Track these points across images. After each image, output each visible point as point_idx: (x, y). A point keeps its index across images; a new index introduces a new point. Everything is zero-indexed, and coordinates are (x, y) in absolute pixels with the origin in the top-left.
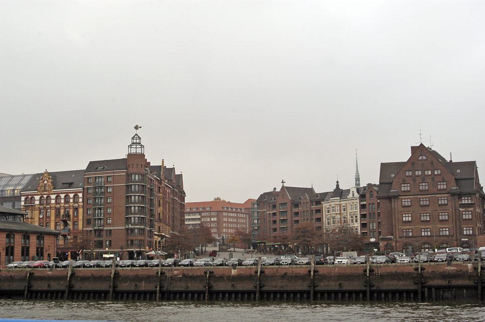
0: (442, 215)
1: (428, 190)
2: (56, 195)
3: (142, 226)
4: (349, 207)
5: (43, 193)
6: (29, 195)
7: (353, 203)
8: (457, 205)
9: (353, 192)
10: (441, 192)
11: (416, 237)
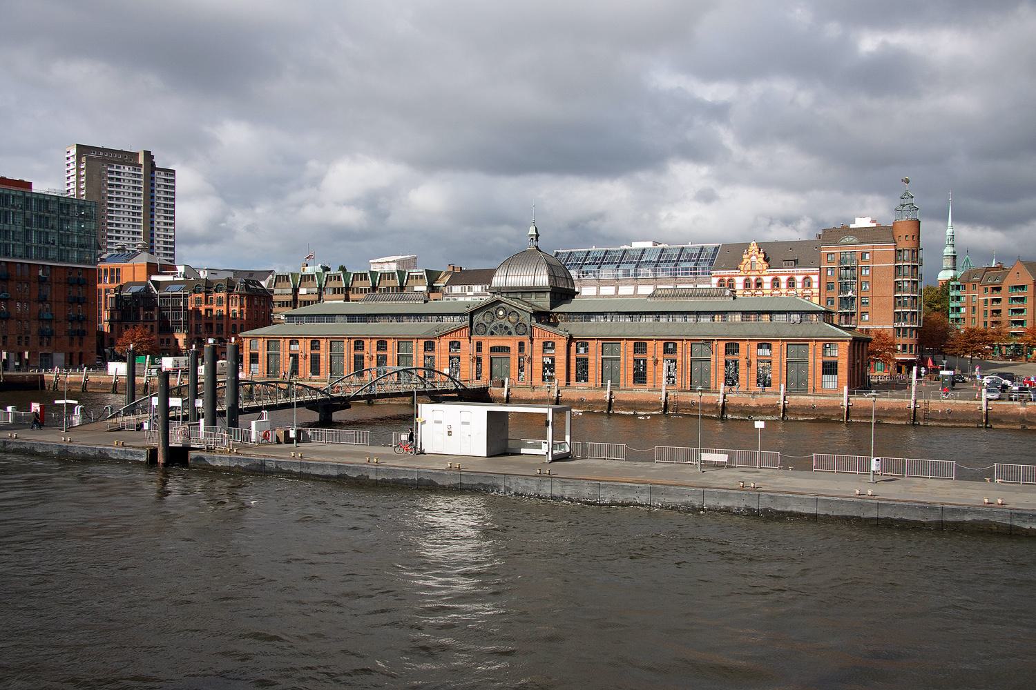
2: (719, 278)
5: (749, 273)
6: (725, 276)
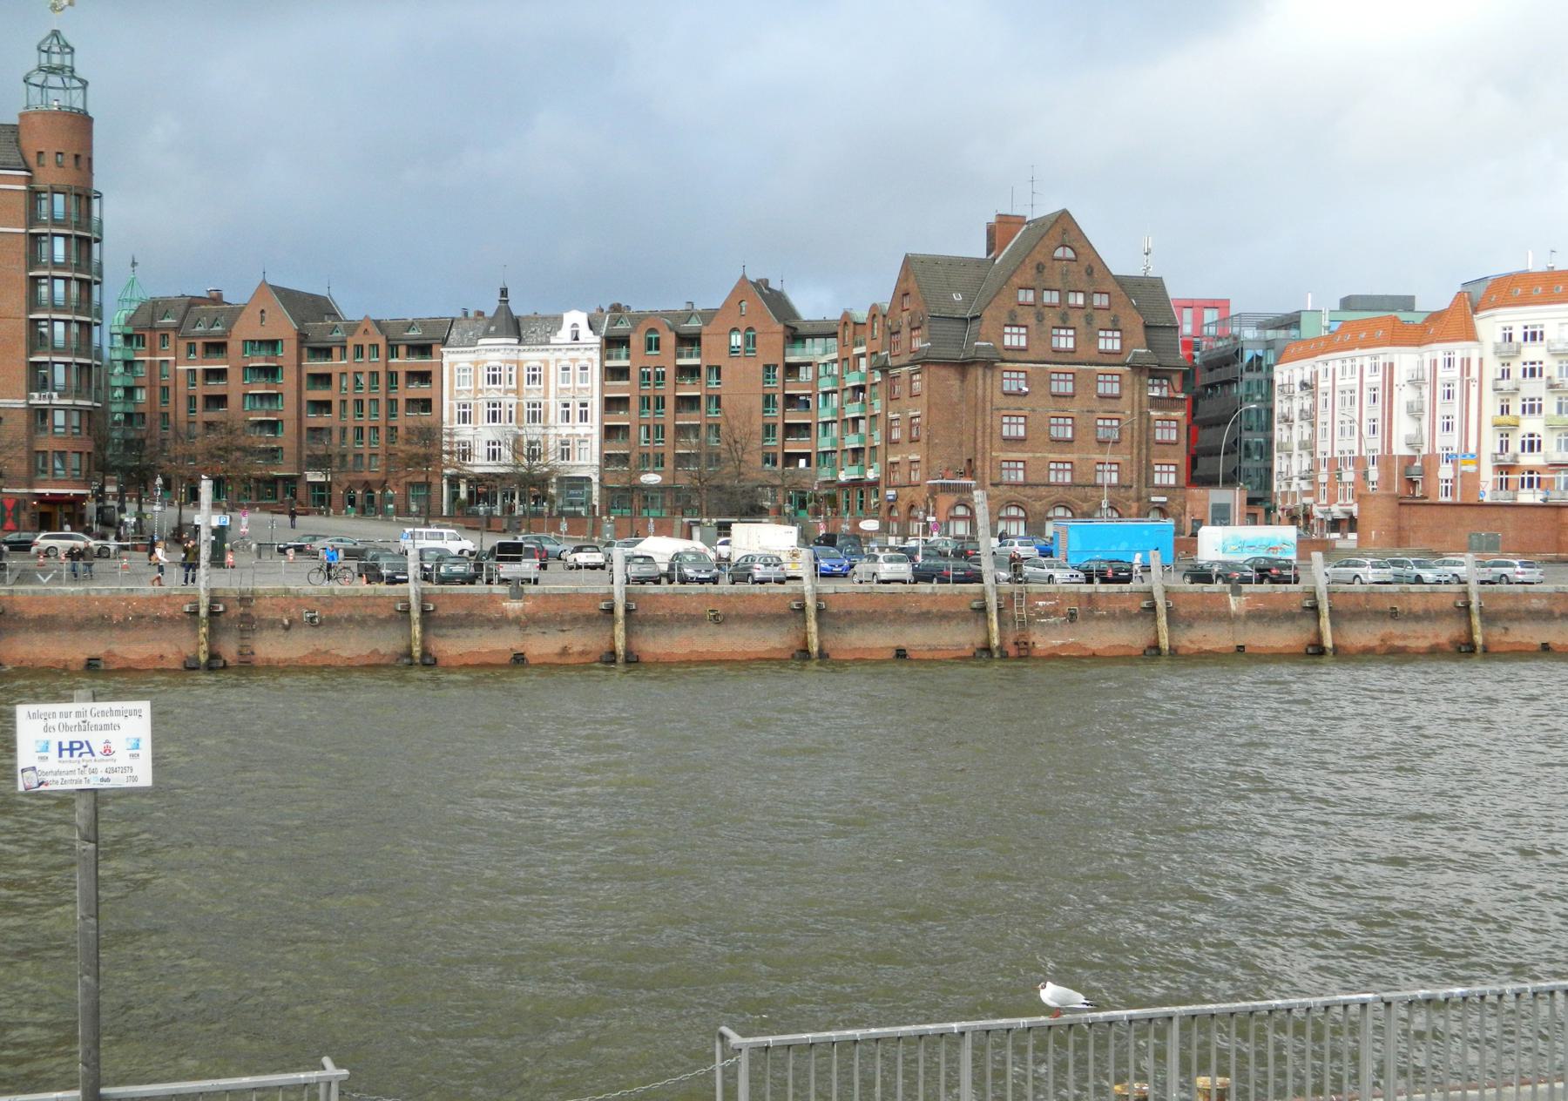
0: (1010, 424)
1: (1073, 352)
3: (82, 398)
4: (554, 375)
7: (574, 360)
8: (1145, 401)
9: (575, 325)
10: (1107, 359)
11: (1037, 485)
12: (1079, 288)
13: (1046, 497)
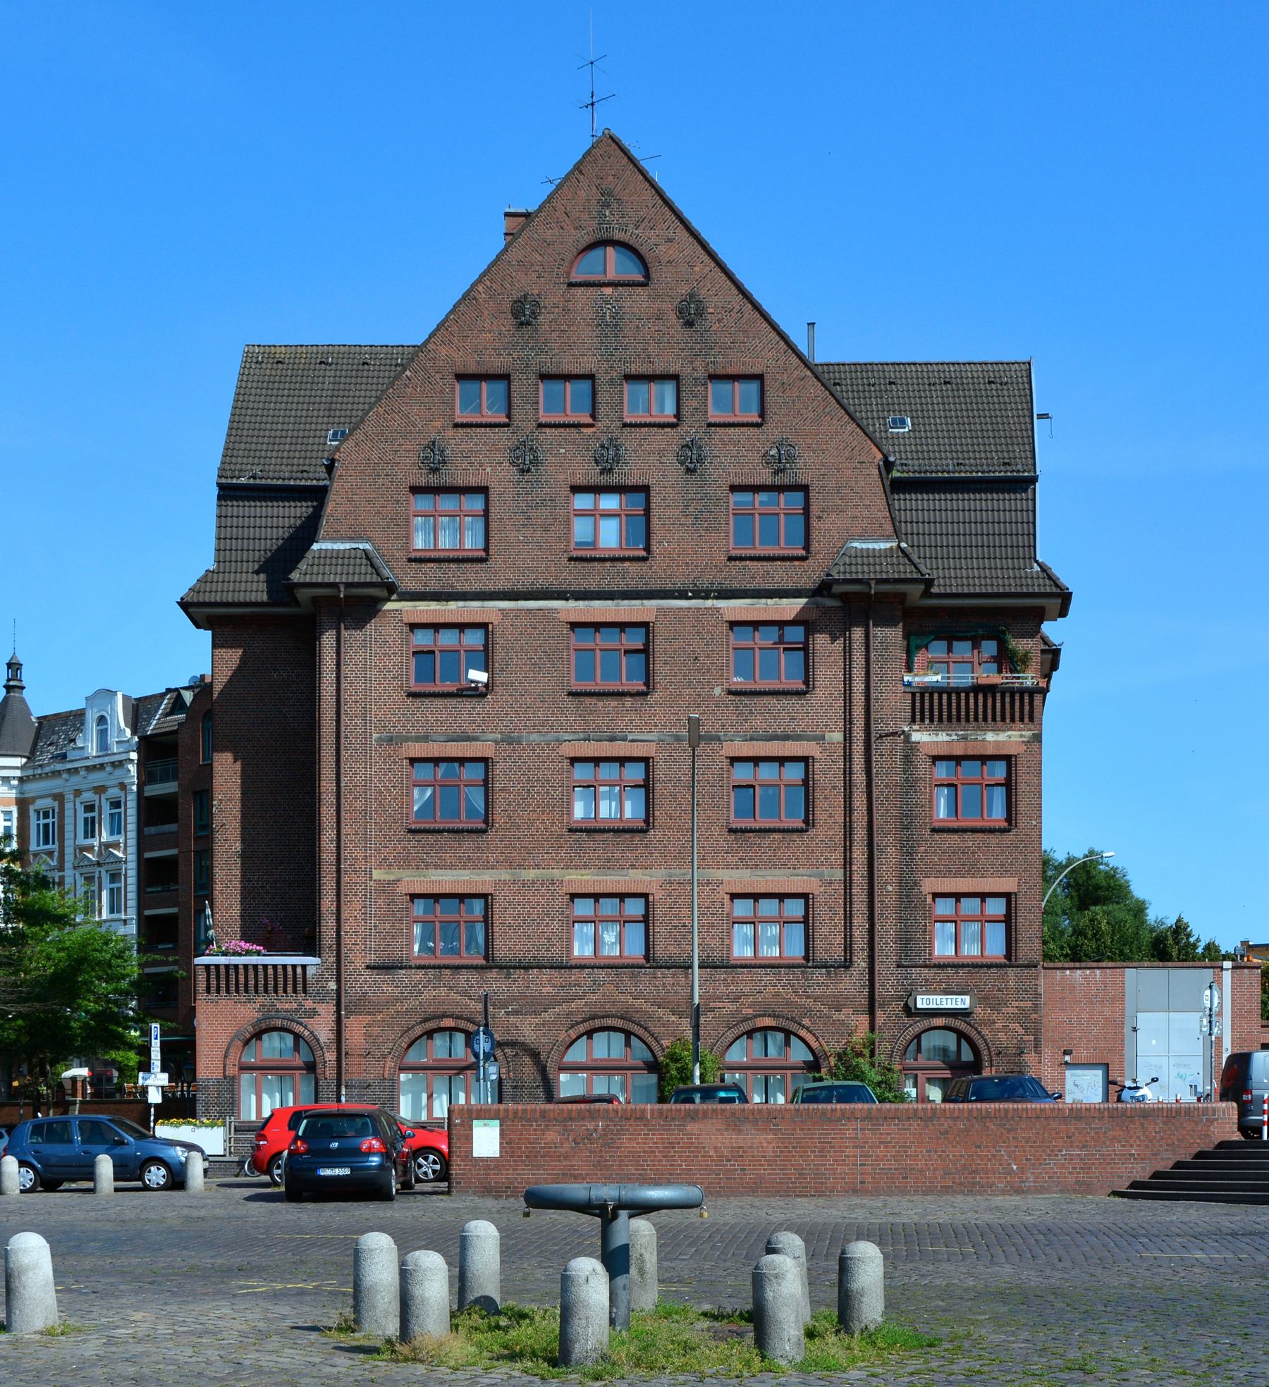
7: (100, 790)
12: (659, 368)
13: (555, 1002)
